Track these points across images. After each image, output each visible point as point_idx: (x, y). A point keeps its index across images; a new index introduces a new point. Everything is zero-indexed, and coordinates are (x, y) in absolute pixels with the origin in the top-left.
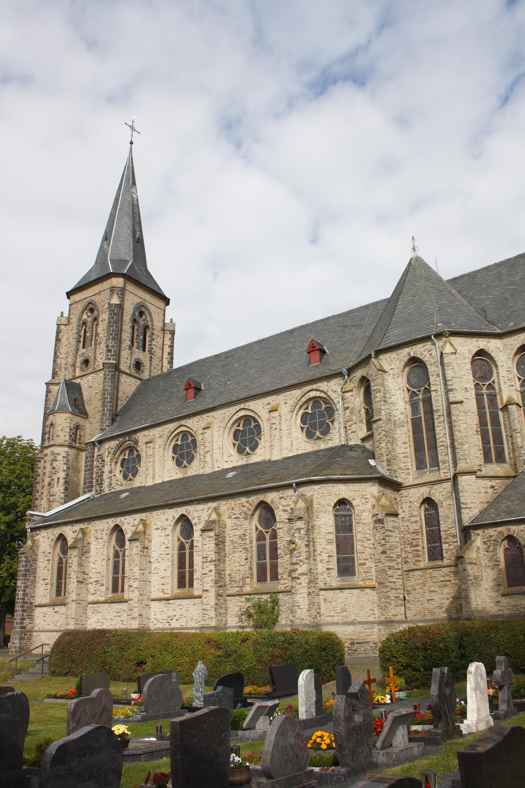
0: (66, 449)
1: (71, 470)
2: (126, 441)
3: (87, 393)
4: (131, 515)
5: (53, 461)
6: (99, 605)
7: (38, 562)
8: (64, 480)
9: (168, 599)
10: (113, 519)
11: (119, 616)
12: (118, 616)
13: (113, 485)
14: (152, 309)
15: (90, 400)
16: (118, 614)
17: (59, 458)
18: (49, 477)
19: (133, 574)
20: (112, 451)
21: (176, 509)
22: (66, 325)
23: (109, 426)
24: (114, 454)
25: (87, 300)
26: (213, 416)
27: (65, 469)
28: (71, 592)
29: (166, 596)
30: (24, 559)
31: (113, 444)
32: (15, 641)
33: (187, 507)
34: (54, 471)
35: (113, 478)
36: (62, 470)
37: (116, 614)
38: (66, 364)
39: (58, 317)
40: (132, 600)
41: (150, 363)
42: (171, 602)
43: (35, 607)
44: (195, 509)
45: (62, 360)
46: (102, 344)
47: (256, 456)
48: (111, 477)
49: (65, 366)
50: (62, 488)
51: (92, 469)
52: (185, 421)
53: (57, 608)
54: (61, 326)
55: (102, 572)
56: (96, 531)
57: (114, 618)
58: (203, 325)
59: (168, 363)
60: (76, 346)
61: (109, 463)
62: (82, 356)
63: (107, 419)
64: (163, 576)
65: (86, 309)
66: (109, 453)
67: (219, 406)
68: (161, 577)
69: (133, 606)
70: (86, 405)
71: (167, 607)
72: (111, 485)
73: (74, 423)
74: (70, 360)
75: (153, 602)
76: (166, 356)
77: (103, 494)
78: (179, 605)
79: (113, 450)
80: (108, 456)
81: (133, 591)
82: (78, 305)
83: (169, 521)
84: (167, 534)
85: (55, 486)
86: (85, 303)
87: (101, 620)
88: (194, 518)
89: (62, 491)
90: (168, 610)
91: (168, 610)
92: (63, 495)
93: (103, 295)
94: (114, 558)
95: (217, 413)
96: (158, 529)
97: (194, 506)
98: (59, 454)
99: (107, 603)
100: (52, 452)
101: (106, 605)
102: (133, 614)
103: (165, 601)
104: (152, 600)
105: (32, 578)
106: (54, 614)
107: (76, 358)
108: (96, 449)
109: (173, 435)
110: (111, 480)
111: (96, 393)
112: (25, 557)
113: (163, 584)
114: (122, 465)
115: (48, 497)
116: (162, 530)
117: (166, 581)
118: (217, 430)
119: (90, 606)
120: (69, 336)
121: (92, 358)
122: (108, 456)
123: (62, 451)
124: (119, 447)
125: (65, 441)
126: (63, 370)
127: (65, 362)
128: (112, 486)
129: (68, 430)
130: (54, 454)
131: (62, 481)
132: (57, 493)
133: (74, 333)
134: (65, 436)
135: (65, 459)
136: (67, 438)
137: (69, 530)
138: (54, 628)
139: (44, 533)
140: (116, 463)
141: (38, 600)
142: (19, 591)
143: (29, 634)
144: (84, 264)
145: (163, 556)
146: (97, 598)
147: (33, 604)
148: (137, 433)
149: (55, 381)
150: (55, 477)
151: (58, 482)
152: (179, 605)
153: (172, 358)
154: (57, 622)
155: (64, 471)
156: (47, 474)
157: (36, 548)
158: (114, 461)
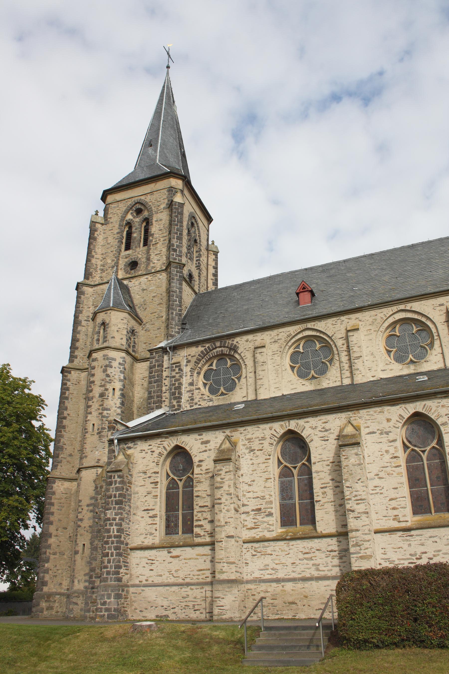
0: (123, 354)
1: (127, 381)
2: (216, 348)
3: (139, 297)
4: (317, 416)
5: (106, 366)
6: (266, 544)
7: (132, 486)
8: (120, 392)
9: (409, 530)
10: (282, 423)
11: (311, 559)
12: (307, 559)
13: (196, 400)
14: (200, 225)
15: (145, 304)
16: (306, 556)
17: (115, 364)
18: (100, 386)
19: (355, 493)
20: (194, 359)
21: (403, 406)
22: (102, 224)
23: (178, 333)
24: (197, 363)
25: (133, 199)
26: (357, 318)
27: (122, 378)
28: (223, 523)
29: (403, 525)
30: (119, 480)
31: (195, 351)
32: (108, 601)
33: (423, 403)
34: (108, 379)
35: (196, 393)
36: (118, 379)
37: (301, 556)
38: (103, 266)
39: (92, 216)
40: (357, 530)
41: (199, 279)
42: (413, 532)
43: (131, 549)
44: (441, 404)
45: (98, 260)
46: (158, 245)
47: (429, 364)
48: (193, 391)
49: (102, 267)
50: (118, 402)
51: (159, 381)
52: (313, 323)
53: (176, 552)
54: (97, 225)
55: (267, 497)
56: (250, 440)
57: (298, 562)
58: (242, 254)
59: (213, 285)
60: (118, 247)
61: (189, 374)
62: (126, 258)
63: (176, 325)
64: (393, 496)
65: (131, 208)
66: (189, 361)
67: (369, 306)
68: (388, 499)
69: (359, 539)
70: (138, 310)
71: (407, 540)
72: (192, 399)
73: (130, 326)
74: (109, 261)
75: (379, 535)
76: (210, 277)
77: (182, 410)
78: (431, 537)
79: (195, 358)
80: (187, 365)
81: (356, 518)
82: (120, 204)
83: (394, 421)
84: (391, 439)
85: (110, 398)
86: (130, 203)
87: (272, 565)
88: (439, 416)
89: (118, 405)
90: (410, 545)
91: (410, 545)
92: (119, 411)
93: (156, 195)
94: (279, 478)
95: (363, 315)
96: (374, 433)
97: (436, 401)
98: (115, 360)
99: (285, 539)
100: (104, 356)
101: (282, 543)
102: (362, 551)
103: (401, 533)
104: (376, 532)
105: (127, 508)
106: (172, 560)
107: (119, 259)
108: (166, 357)
109: (294, 340)
110: (192, 394)
111: (154, 297)
112: (119, 477)
113: (394, 509)
114: (206, 377)
115: (101, 411)
116: (381, 434)
117: (399, 503)
118: (366, 333)
119: (246, 545)
120: (109, 237)
121: (144, 260)
122: (187, 365)
123: (118, 356)
124: (203, 355)
125: (122, 345)
126: (99, 272)
127: (102, 263)
128: (194, 402)
129: (125, 332)
130: (108, 359)
131: (118, 393)
132: (112, 407)
133: (115, 233)
134: (122, 339)
135: (122, 367)
136: (124, 342)
137: (193, 441)
138: (172, 580)
139: (142, 445)
140: (199, 373)
141: (135, 541)
142: (111, 525)
143: (126, 589)
144: (124, 166)
145: (389, 469)
146: (261, 534)
147: (129, 546)
148: (234, 338)
149: (87, 282)
150: (110, 387)
151: (114, 394)
152: (431, 537)
153: (216, 280)
154: (177, 571)
155: (120, 380)
156: (98, 383)
157: (131, 465)
158: (196, 371)
